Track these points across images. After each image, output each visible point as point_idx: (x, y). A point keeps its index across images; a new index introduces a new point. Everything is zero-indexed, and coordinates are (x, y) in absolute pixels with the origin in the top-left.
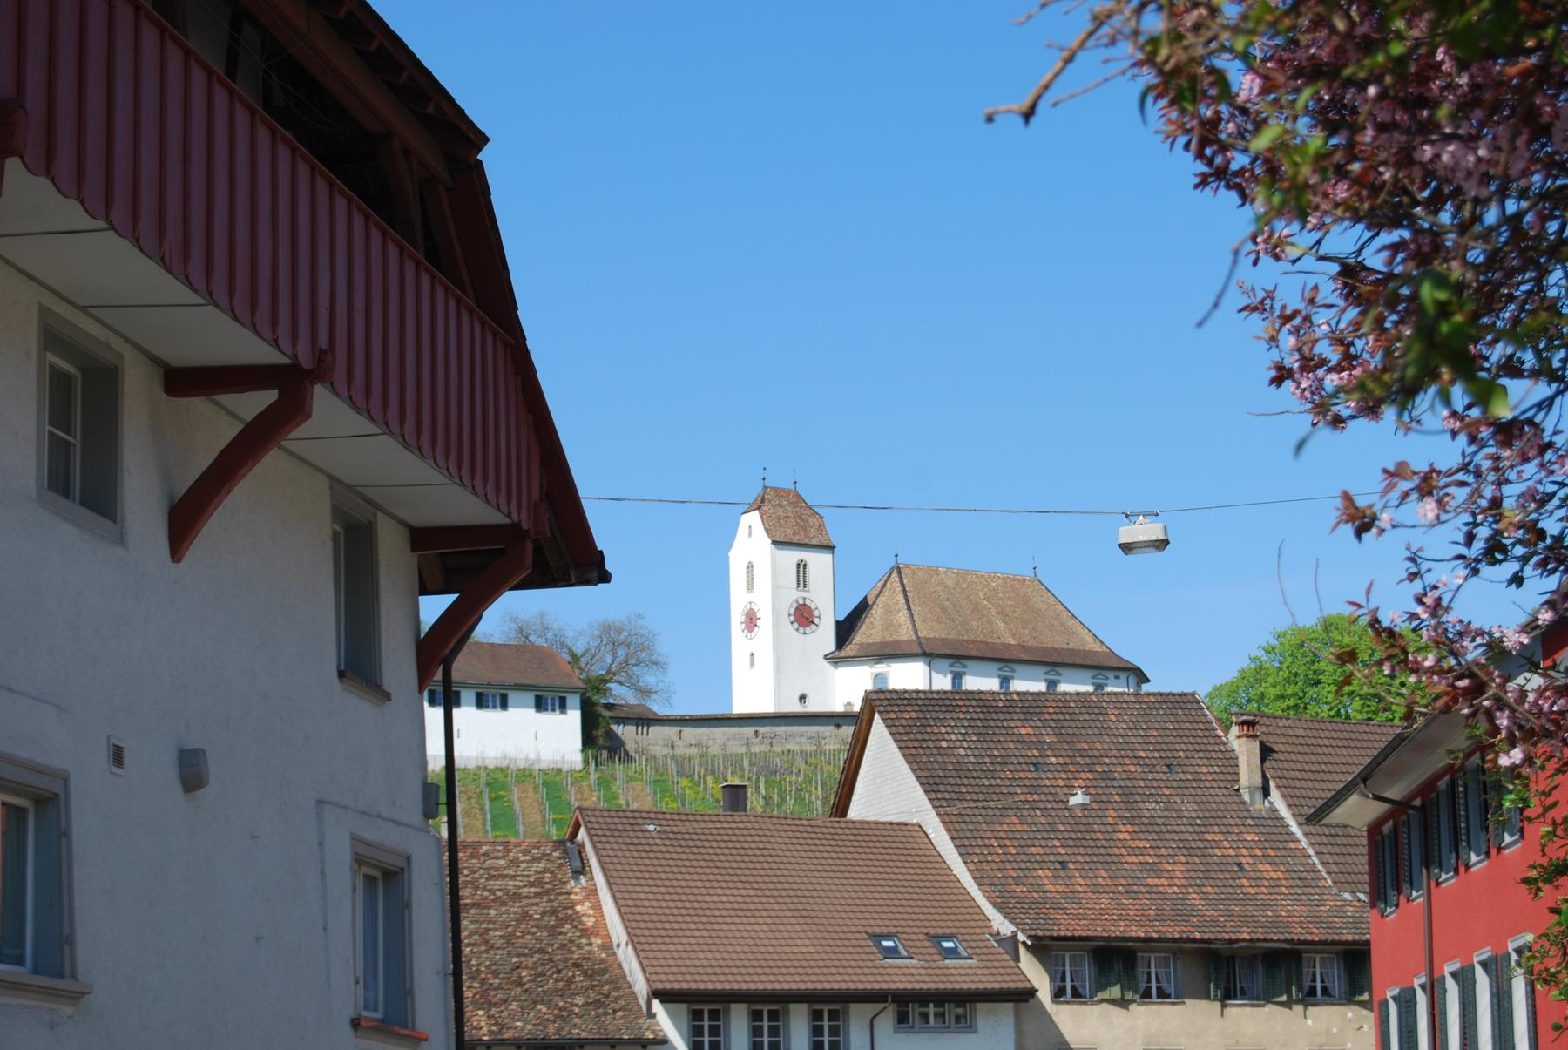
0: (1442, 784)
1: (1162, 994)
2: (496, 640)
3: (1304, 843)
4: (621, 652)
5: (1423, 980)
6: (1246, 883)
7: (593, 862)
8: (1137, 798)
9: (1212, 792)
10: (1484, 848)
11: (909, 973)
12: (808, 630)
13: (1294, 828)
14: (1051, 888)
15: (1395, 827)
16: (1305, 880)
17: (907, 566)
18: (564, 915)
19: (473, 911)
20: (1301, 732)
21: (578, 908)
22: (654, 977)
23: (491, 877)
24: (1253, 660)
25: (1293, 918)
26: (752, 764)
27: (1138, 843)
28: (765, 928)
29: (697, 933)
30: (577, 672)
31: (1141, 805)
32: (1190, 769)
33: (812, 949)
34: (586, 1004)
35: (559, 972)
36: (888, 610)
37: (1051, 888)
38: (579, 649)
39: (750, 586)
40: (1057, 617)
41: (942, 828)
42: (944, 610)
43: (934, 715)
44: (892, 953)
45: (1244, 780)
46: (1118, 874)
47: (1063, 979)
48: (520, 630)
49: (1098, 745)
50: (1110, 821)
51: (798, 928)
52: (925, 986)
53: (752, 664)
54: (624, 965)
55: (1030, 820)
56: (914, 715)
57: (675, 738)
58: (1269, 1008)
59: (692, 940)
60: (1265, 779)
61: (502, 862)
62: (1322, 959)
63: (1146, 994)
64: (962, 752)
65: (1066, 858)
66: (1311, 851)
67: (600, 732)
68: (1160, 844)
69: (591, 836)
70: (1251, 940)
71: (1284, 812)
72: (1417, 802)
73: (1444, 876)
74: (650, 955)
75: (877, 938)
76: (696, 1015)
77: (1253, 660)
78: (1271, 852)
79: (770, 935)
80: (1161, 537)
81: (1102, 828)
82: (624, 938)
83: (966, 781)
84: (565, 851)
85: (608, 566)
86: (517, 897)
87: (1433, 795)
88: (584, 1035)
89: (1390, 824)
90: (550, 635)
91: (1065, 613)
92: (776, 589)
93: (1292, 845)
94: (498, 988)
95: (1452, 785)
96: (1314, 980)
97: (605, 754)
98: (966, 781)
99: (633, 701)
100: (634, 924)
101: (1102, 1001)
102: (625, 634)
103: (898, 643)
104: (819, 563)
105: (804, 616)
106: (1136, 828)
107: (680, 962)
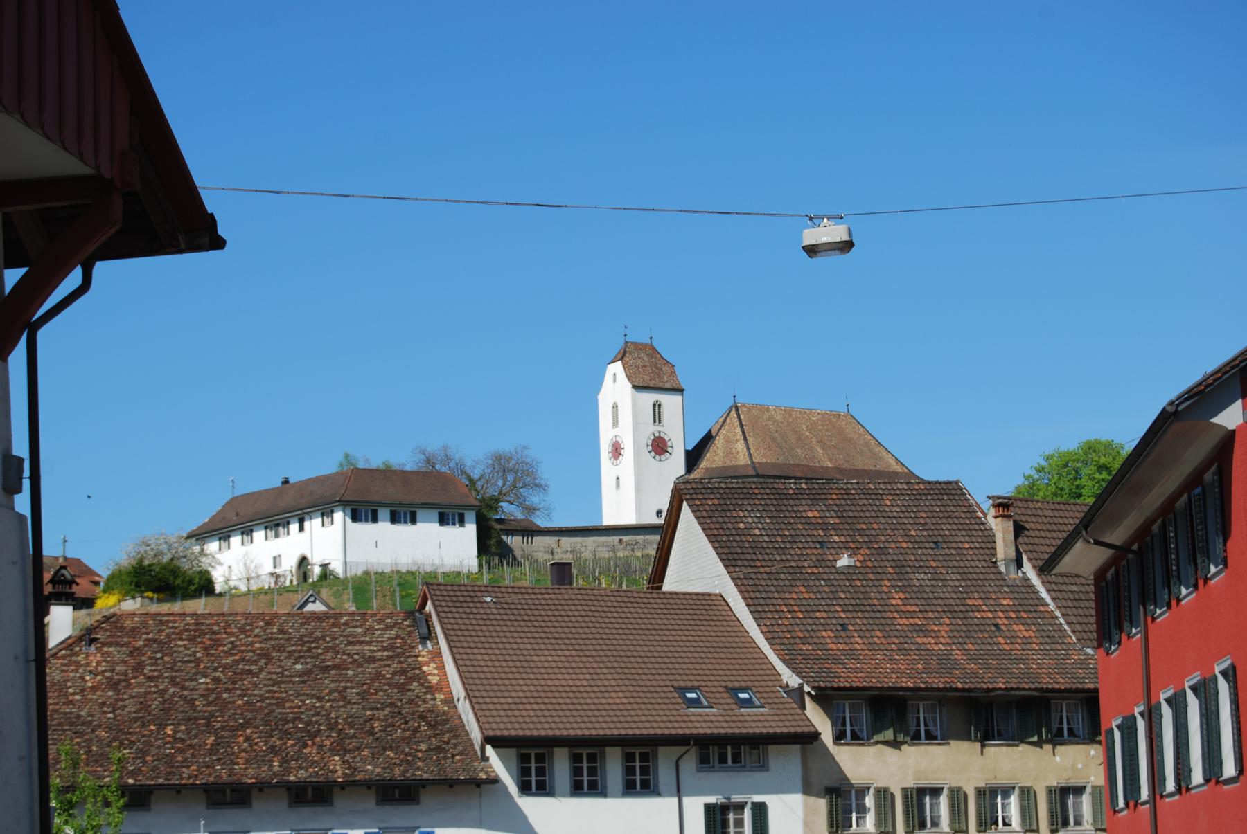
0: (1155, 528)
1: (930, 737)
2: (408, 468)
3: (1052, 606)
4: (510, 478)
5: (1142, 708)
6: (1002, 641)
7: (438, 629)
8: (908, 569)
9: (973, 564)
10: (1192, 581)
11: (709, 719)
12: (663, 457)
13: (1044, 594)
14: (833, 646)
15: (1117, 571)
16: (1053, 637)
17: (743, 405)
18: (412, 674)
19: (333, 672)
20: (1049, 513)
21: (425, 668)
22: (487, 726)
23: (350, 643)
24: (1027, 478)
25: (1041, 669)
26: (616, 565)
27: (911, 609)
28: (585, 683)
29: (525, 688)
30: (474, 493)
31: (912, 576)
32: (954, 545)
33: (625, 701)
34: (429, 750)
35: (406, 723)
36: (728, 441)
37: (833, 646)
38: (475, 475)
39: (615, 423)
40: (867, 444)
41: (739, 597)
42: (774, 440)
43: (734, 501)
44: (695, 703)
45: (1000, 554)
46: (891, 634)
47: (844, 724)
48: (428, 460)
49: (875, 526)
50: (885, 589)
51: (613, 683)
52: (722, 731)
53: (618, 485)
54: (463, 717)
55: (815, 589)
56: (716, 502)
57: (554, 546)
58: (1023, 748)
59: (521, 694)
60: (1019, 553)
61: (359, 630)
62: (1068, 705)
63: (916, 737)
64: (757, 532)
65: (847, 621)
66: (1058, 613)
67: (493, 542)
68: (927, 608)
69: (435, 607)
70: (1006, 689)
71: (1035, 580)
72: (1135, 547)
73: (1158, 611)
74: (484, 707)
75: (682, 690)
76: (524, 759)
77: (1027, 478)
78: (1023, 614)
79: (589, 689)
80: (846, 238)
81: (878, 596)
82: (463, 694)
83: (760, 557)
84: (414, 620)
85: (222, 231)
86: (372, 660)
87: (1148, 539)
88: (425, 776)
89: (1112, 570)
90: (452, 464)
91: (873, 442)
92: (636, 425)
93: (1042, 608)
94: (354, 737)
95: (1164, 529)
96: (1061, 723)
97: (497, 561)
98: (760, 557)
99: (520, 516)
100: (471, 681)
101: (877, 743)
102: (513, 462)
103: (735, 467)
104: (671, 403)
105: (659, 447)
106: (908, 596)
107: (510, 713)
